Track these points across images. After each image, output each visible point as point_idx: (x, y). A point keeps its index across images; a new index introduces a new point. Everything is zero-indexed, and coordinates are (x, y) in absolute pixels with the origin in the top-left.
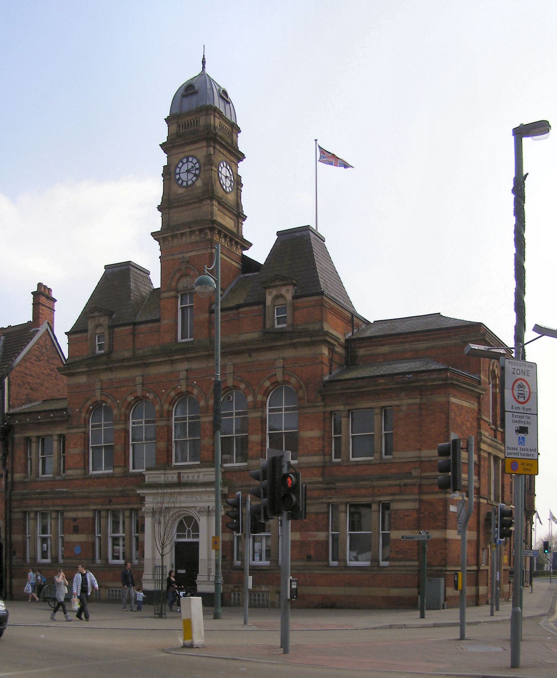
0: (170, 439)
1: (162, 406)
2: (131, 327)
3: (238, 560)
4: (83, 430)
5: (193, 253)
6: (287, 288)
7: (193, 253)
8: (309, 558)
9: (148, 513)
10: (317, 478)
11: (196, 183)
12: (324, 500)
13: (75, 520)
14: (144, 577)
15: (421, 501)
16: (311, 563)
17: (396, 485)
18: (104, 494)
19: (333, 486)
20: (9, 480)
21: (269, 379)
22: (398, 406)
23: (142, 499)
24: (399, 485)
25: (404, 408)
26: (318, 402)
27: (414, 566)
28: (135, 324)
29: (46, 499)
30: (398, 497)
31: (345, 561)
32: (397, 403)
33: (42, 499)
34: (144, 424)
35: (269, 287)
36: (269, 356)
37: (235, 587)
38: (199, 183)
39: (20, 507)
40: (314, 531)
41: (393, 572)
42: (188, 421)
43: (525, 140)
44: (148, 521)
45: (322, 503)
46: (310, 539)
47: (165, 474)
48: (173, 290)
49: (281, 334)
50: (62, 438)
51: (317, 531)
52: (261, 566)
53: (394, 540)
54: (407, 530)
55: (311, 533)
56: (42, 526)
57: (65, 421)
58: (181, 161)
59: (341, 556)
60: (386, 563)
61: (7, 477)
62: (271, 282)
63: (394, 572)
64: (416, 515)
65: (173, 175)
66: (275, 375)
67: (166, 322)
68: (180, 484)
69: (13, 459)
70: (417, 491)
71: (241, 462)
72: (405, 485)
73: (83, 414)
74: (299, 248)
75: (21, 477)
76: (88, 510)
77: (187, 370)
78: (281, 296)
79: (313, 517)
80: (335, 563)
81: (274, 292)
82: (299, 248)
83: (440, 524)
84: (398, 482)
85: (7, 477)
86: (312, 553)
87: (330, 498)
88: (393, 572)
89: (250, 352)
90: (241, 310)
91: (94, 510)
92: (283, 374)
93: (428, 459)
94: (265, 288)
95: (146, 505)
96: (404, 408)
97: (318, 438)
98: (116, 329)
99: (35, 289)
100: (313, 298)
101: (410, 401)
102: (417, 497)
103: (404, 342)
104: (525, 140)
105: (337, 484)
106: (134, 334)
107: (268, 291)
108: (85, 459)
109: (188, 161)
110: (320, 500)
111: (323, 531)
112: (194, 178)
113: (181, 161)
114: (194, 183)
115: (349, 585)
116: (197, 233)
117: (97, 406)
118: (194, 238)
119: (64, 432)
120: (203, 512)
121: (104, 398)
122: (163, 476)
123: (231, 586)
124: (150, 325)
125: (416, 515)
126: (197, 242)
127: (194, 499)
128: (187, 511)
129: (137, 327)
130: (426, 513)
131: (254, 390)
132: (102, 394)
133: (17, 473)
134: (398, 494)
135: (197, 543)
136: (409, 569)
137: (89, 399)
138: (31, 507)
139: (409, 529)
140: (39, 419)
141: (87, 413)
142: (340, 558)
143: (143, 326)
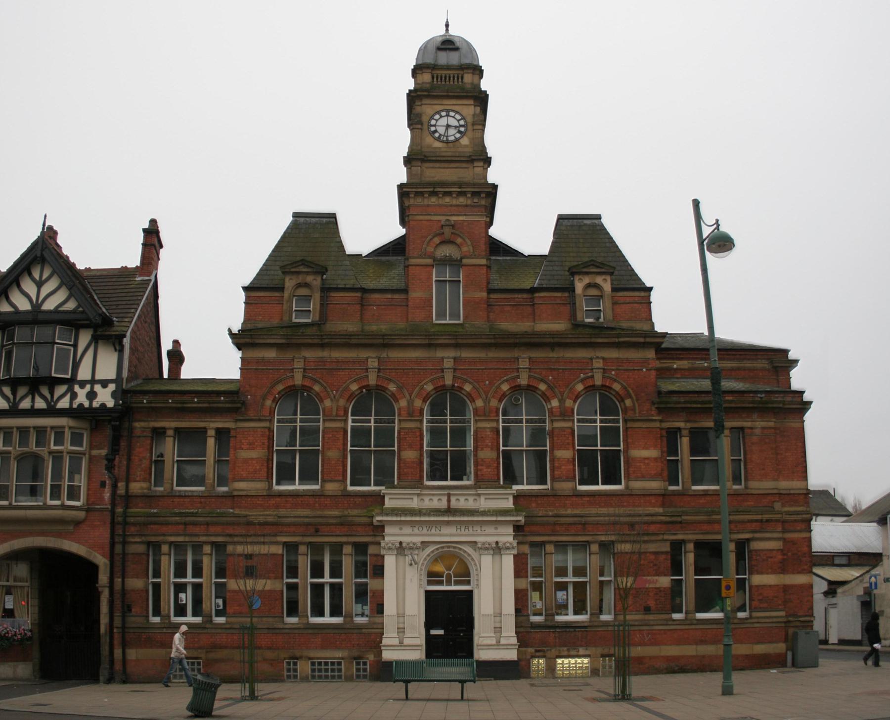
0: (345, 449)
1: (410, 402)
2: (359, 294)
3: (154, 615)
4: (267, 424)
5: (461, 218)
6: (604, 277)
7: (461, 218)
8: (647, 610)
9: (390, 549)
10: (656, 509)
11: (461, 141)
12: (666, 537)
13: (249, 556)
14: (385, 641)
15: (784, 540)
16: (651, 617)
17: (757, 521)
18: (307, 520)
19: (679, 519)
20: (121, 490)
21: (582, 381)
22: (751, 428)
23: (380, 529)
24: (761, 521)
25: (758, 432)
26: (652, 415)
27: (781, 617)
28: (364, 290)
29: (195, 524)
30: (757, 535)
31: (169, 617)
32: (749, 424)
33: (186, 524)
34: (372, 424)
35: (579, 273)
36: (582, 354)
37: (536, 651)
38: (465, 141)
39: (142, 535)
40: (654, 575)
41: (756, 625)
42: (449, 425)
43: (134, 261)
44: (390, 562)
45: (666, 540)
46: (647, 586)
47: (418, 495)
48: (430, 257)
49: (597, 329)
50: (222, 435)
51: (658, 575)
52: (578, 622)
53: (756, 586)
54: (771, 573)
55: (649, 578)
56: (721, 557)
57: (236, 410)
58: (448, 111)
59: (164, 611)
60: (221, 620)
61: (115, 487)
62: (584, 267)
63: (758, 625)
64: (780, 557)
65: (425, 126)
66: (592, 377)
67: (416, 294)
68: (449, 511)
69: (129, 460)
70: (780, 529)
71: (537, 484)
72: (767, 521)
73: (269, 403)
74: (583, 240)
75: (142, 488)
76: (277, 543)
77: (455, 358)
78: (596, 286)
79: (652, 557)
80: (157, 620)
81: (587, 280)
82: (583, 240)
83: (806, 567)
84: (759, 517)
85: (115, 487)
86: (652, 603)
87: (675, 534)
88: (756, 625)
89: (553, 346)
90: (537, 295)
91: (286, 544)
92: (604, 377)
93: (788, 492)
94: (573, 274)
95: (387, 538)
96: (758, 432)
97: (656, 459)
98: (333, 294)
99: (147, 226)
100: (637, 294)
101: (763, 424)
102: (780, 535)
103: (744, 359)
104: (134, 261)
105: (684, 517)
106: (363, 304)
107: (577, 278)
108: (268, 466)
109: (448, 115)
110: (661, 537)
111: (665, 575)
112: (458, 135)
113: (438, 113)
114: (457, 140)
115: (702, 642)
116: (469, 195)
117: (292, 392)
118: (462, 200)
119: (229, 425)
120: (487, 549)
121: (307, 383)
122: (415, 498)
123: (531, 650)
124: (389, 296)
125: (780, 557)
126: (466, 206)
127: (479, 531)
128: (460, 549)
129: (367, 295)
130: (790, 554)
131: (562, 394)
132: (304, 377)
133: (135, 481)
134: (760, 532)
135: (470, 594)
136: (775, 620)
137: (280, 382)
138: (164, 535)
139: (774, 572)
140: (195, 403)
141: (273, 401)
142: (162, 613)
143: (377, 296)
